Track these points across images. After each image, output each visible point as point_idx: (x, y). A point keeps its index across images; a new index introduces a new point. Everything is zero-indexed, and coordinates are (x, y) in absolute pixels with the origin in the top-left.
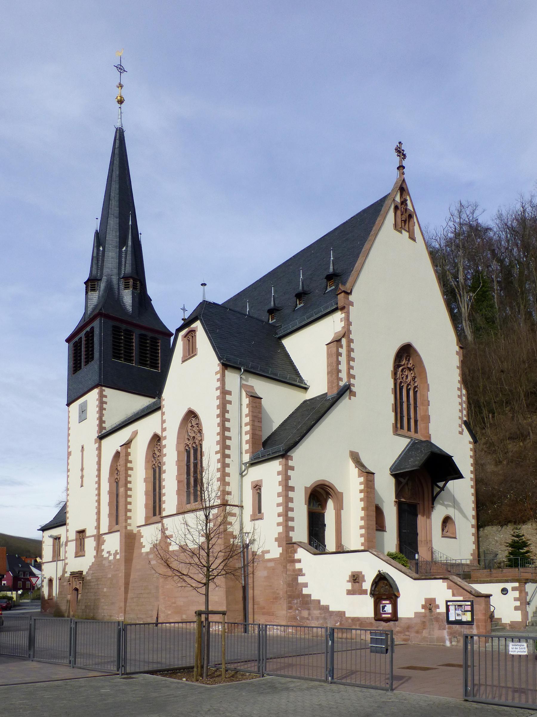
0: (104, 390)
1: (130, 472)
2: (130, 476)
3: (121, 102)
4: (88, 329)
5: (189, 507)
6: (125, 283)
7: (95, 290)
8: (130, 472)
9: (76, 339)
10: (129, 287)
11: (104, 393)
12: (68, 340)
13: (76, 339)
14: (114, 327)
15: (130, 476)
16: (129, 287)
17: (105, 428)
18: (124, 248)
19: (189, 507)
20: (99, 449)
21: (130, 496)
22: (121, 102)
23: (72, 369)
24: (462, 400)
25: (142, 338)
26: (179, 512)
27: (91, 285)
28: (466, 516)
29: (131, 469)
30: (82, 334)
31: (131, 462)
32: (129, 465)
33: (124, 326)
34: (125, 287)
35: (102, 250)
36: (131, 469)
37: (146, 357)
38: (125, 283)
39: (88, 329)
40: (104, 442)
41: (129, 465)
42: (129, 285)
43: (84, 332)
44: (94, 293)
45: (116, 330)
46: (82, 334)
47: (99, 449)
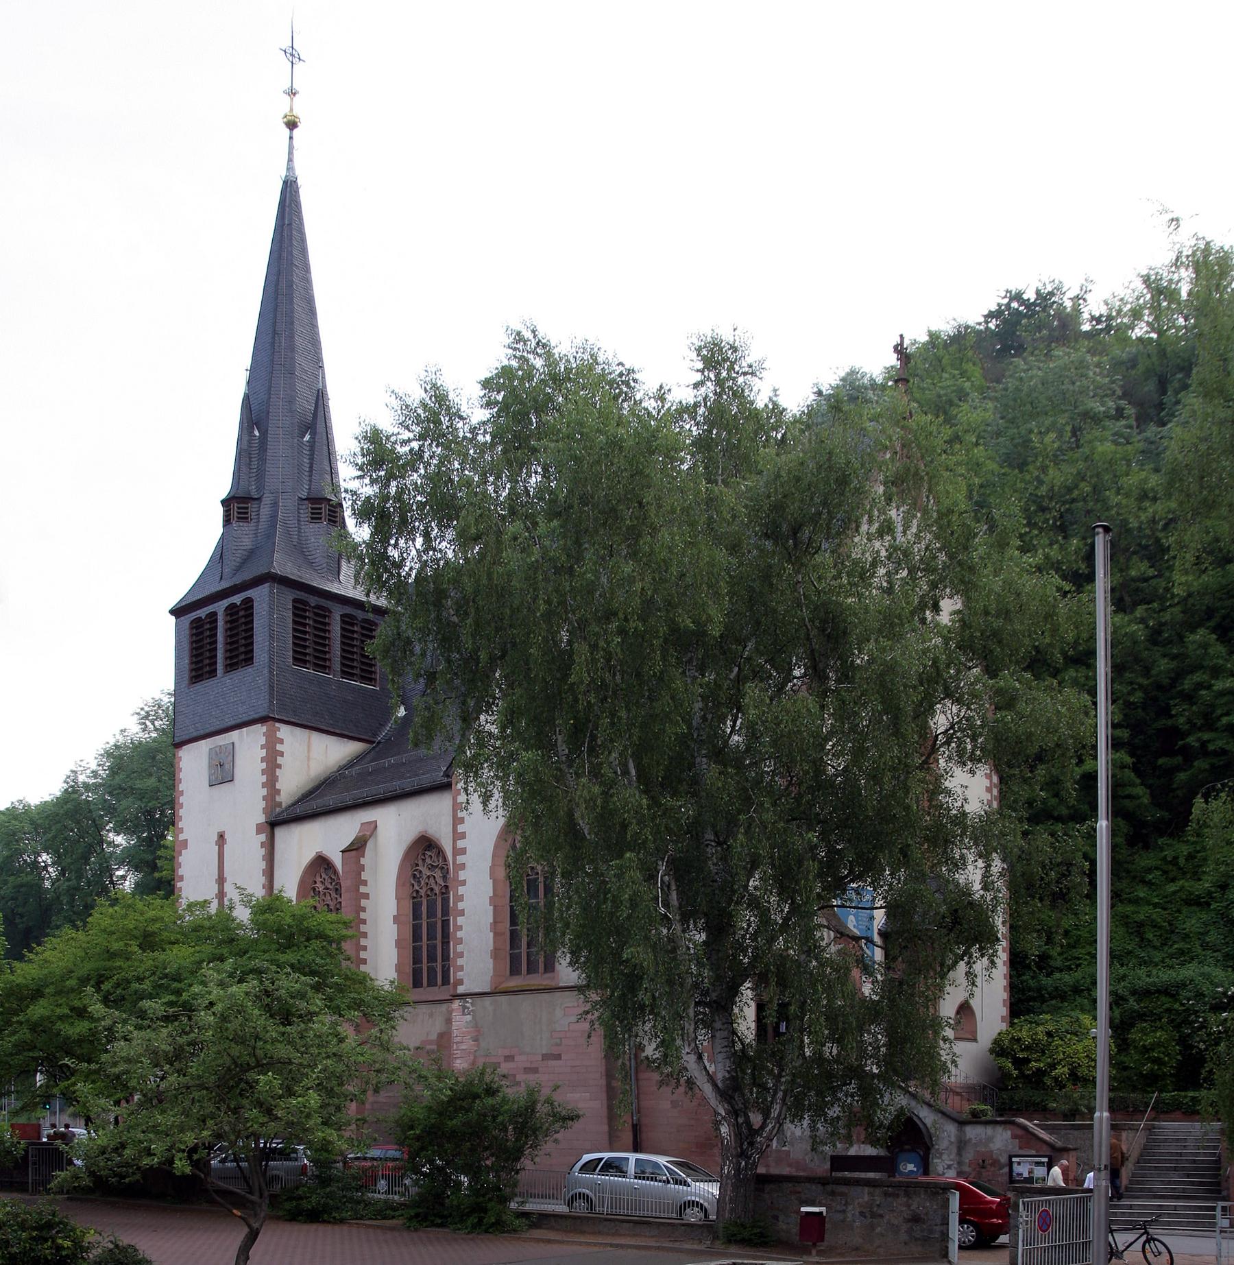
0: (279, 729)
1: (364, 902)
2: (364, 910)
3: (292, 125)
4: (237, 599)
5: (515, 982)
6: (312, 509)
7: (247, 518)
8: (364, 902)
9: (202, 613)
10: (320, 518)
11: (279, 735)
12: (177, 612)
13: (202, 613)
14: (295, 601)
15: (364, 910)
16: (320, 518)
17: (280, 804)
18: (307, 437)
19: (515, 982)
20: (270, 848)
21: (365, 948)
22: (292, 125)
23: (186, 675)
24: (991, 781)
25: (347, 620)
26: (497, 990)
27: (239, 508)
28: (608, 1092)
29: (366, 896)
30: (220, 607)
31: (365, 883)
32: (363, 889)
33: (313, 600)
34: (312, 518)
35: (260, 437)
36: (366, 896)
37: (305, 647)
38: (312, 509)
39: (237, 599)
40: (280, 833)
41: (363, 889)
42: (321, 514)
43: (225, 603)
44: (245, 524)
45: (299, 609)
46: (220, 607)
47: (270, 848)
